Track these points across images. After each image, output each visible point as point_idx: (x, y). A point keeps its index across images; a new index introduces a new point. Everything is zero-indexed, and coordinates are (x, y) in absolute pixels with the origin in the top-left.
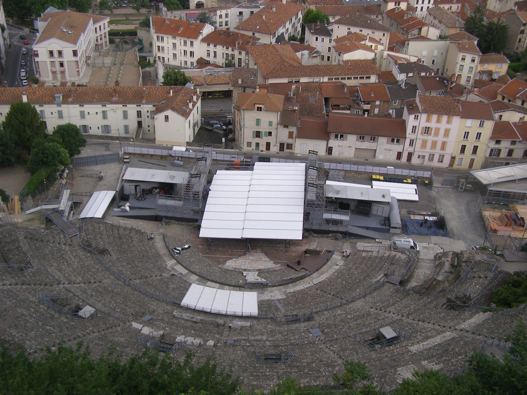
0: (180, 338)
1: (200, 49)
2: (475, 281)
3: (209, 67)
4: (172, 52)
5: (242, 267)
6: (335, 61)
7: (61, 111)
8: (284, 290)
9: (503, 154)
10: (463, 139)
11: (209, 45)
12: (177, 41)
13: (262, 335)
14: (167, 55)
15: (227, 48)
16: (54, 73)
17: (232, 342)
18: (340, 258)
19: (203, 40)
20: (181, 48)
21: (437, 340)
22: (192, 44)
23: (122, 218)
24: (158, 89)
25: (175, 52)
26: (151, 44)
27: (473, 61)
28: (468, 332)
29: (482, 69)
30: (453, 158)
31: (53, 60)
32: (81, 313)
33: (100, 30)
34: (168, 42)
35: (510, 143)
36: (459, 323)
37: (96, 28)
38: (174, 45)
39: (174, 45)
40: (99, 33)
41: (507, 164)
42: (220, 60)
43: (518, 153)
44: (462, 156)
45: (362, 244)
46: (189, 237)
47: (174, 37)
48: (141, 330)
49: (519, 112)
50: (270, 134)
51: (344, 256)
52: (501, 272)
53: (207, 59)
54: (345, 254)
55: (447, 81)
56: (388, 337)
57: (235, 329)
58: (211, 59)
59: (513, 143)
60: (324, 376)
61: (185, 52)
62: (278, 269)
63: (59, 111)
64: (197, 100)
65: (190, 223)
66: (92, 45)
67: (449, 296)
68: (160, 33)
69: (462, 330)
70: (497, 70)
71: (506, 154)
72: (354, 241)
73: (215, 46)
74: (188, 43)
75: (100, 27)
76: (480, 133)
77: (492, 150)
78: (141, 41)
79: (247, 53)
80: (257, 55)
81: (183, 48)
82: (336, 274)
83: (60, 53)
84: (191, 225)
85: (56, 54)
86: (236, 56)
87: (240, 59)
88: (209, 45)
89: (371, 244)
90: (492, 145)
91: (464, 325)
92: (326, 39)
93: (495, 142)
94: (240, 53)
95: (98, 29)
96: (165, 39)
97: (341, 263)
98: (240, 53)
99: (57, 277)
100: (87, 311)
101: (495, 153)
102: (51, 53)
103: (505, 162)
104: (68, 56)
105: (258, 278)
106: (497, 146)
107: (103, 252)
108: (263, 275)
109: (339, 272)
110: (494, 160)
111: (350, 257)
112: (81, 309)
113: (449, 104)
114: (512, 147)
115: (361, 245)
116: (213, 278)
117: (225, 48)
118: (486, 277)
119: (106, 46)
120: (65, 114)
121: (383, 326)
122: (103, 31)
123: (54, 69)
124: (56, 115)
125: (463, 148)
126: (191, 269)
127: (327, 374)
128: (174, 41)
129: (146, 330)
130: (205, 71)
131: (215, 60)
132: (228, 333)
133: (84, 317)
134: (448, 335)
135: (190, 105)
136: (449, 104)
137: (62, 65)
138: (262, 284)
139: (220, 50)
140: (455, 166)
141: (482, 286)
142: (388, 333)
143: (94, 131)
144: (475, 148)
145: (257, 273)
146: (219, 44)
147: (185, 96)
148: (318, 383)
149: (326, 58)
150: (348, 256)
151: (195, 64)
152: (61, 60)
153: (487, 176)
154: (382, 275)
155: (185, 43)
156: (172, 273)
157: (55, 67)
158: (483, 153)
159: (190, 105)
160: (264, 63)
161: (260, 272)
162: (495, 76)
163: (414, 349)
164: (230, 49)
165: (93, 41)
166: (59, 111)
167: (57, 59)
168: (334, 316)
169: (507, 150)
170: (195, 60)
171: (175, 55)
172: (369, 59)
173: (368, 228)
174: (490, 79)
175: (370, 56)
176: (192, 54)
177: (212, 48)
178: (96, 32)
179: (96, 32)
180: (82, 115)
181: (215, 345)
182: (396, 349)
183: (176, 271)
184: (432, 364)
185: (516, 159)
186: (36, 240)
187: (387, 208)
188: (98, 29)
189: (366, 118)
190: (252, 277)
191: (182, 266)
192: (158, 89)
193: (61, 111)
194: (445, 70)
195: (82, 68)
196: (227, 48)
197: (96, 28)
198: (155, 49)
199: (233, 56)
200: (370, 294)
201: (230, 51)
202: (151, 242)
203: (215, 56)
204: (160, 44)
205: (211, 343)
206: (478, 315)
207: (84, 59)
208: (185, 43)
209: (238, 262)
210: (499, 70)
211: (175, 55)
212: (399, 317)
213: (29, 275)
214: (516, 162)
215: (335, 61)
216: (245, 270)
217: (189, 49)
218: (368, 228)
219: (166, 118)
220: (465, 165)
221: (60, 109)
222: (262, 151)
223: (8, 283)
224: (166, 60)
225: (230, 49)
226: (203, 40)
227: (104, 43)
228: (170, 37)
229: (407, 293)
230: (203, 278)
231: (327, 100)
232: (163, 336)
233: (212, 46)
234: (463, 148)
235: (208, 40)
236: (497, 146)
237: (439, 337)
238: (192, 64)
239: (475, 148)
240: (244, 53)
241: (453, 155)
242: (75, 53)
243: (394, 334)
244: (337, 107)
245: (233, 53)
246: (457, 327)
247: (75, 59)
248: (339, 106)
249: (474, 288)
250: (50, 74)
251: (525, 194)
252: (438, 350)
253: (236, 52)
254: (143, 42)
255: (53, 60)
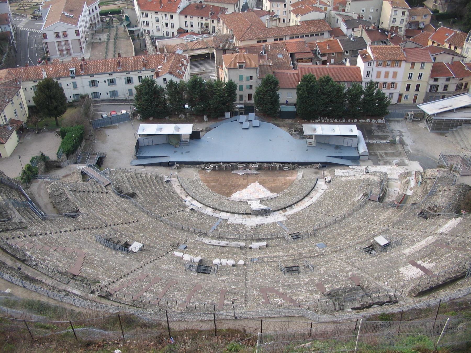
0: (216, 261)
1: (178, 21)
2: (441, 193)
3: (188, 35)
4: (155, 25)
5: (246, 198)
6: (293, 22)
7: (76, 82)
8: (284, 214)
9: (440, 89)
10: (408, 79)
11: (186, 17)
12: (159, 16)
13: (279, 252)
14: (152, 28)
15: (202, 18)
16: (61, 51)
17: (257, 260)
18: (324, 183)
19: (181, 13)
20: (163, 21)
21: (424, 243)
22: (172, 17)
23: (141, 167)
24: (154, 57)
25: (158, 25)
26: (137, 22)
27: (403, 13)
28: (446, 235)
29: (410, 21)
30: (401, 95)
31: (59, 40)
32: (131, 248)
33: (93, 11)
34: (151, 17)
35: (445, 80)
36: (437, 229)
37: (89, 10)
38: (157, 19)
39: (157, 19)
40: (92, 14)
41: (443, 97)
42: (197, 29)
43: (452, 88)
44: (407, 93)
45: (339, 171)
46: (198, 177)
47: (156, 13)
48: (183, 257)
49: (449, 54)
50: (251, 86)
51: (326, 182)
52: (460, 185)
53: (185, 28)
54: (327, 180)
55: (388, 33)
56: (382, 244)
57: (255, 249)
58: (189, 28)
59: (448, 79)
60: (342, 281)
61: (167, 24)
62: (275, 197)
63: (73, 83)
64: (188, 64)
65: (197, 166)
66: (88, 25)
67: (422, 208)
68: (144, 10)
69: (441, 234)
70: (423, 20)
71: (443, 89)
72: (333, 168)
73: (191, 17)
74: (169, 17)
75: (96, 7)
76: (422, 74)
77: (431, 86)
78: (127, 18)
79: (219, 21)
80: (229, 22)
81: (165, 21)
82: (323, 197)
83: (65, 35)
84: (198, 168)
85: (61, 35)
86: (210, 24)
87: (213, 27)
88: (186, 17)
89: (346, 171)
90: (432, 82)
91: (441, 230)
92: (282, 5)
93: (433, 80)
94: (213, 22)
95: (91, 11)
96: (149, 15)
97: (325, 187)
98: (213, 22)
99: (104, 221)
100: (135, 246)
101: (434, 88)
102: (58, 35)
103: (441, 95)
104: (72, 36)
105: (261, 205)
106: (436, 83)
107: (133, 195)
108: (264, 203)
109: (325, 194)
110: (433, 95)
111: (332, 182)
112: (130, 245)
113: (395, 51)
114: (447, 83)
115: (338, 172)
116: (224, 209)
117: (200, 18)
118: (450, 190)
119: (99, 24)
120: (78, 85)
121: (374, 236)
122: (95, 12)
123: (61, 48)
124: (71, 86)
125: (409, 86)
126: (204, 202)
127: (344, 278)
128: (157, 16)
129: (187, 257)
130: (184, 40)
131: (192, 29)
132: (250, 252)
133: (135, 251)
134: (431, 239)
135: (183, 68)
136: (395, 51)
137: (66, 42)
138: (265, 210)
139: (196, 21)
140: (402, 101)
141: (447, 197)
142: (381, 240)
143: (104, 96)
144: (418, 86)
145: (259, 201)
146: (195, 16)
147: (177, 61)
148: (339, 286)
149: (282, 21)
150: (330, 182)
151: (176, 34)
152: (66, 39)
153: (430, 108)
154: (362, 195)
155: (166, 16)
156: (191, 208)
157: (61, 46)
158: (424, 89)
159: (183, 68)
160: (236, 29)
161: (261, 201)
162: (422, 26)
163: (407, 251)
164: (204, 19)
165: (88, 21)
166: (73, 83)
167: (62, 39)
168: (331, 231)
169: (443, 86)
170: (175, 30)
171: (158, 28)
172: (321, 18)
173: (341, 158)
174: (417, 28)
175: (321, 16)
176: (172, 25)
177: (188, 19)
178: (90, 13)
179: (90, 13)
180: (93, 84)
181: (245, 264)
182: (392, 254)
183: (194, 205)
184: (426, 263)
185: (450, 92)
186: (79, 191)
187: (355, 140)
188: (91, 11)
189: (348, 68)
190: (256, 206)
191: (197, 201)
192: (154, 57)
193: (76, 82)
194: (381, 23)
195: (83, 45)
196: (202, 18)
197: (89, 10)
198: (141, 24)
199: (207, 25)
200: (357, 211)
201: (204, 21)
202: (169, 184)
203: (192, 26)
204: (145, 19)
205: (241, 262)
206: (451, 221)
207: (84, 37)
208: (166, 16)
209: (241, 194)
210: (424, 20)
211: (158, 28)
212: (386, 227)
213: (82, 221)
214: (450, 95)
215: (293, 22)
216: (249, 200)
217: (169, 21)
218: (341, 158)
219: (164, 80)
220: (410, 100)
221: (74, 80)
222: (245, 101)
223: (68, 230)
224: (151, 32)
225: (204, 19)
226: (181, 13)
227: (97, 23)
228: (153, 13)
229: (386, 208)
230: (216, 209)
231: (292, 55)
232: (201, 261)
233: (189, 17)
234: (409, 86)
235: (184, 12)
236: (436, 83)
237: (424, 241)
238: (173, 33)
239: (418, 86)
240: (216, 21)
241: (401, 93)
242: (77, 33)
243: (386, 242)
244: (300, 60)
245: (207, 22)
246: (436, 232)
247: (77, 38)
248: (302, 59)
249: (442, 199)
250: (58, 52)
251: (470, 120)
252: (427, 251)
253: (209, 21)
254: (130, 19)
255: (59, 40)
